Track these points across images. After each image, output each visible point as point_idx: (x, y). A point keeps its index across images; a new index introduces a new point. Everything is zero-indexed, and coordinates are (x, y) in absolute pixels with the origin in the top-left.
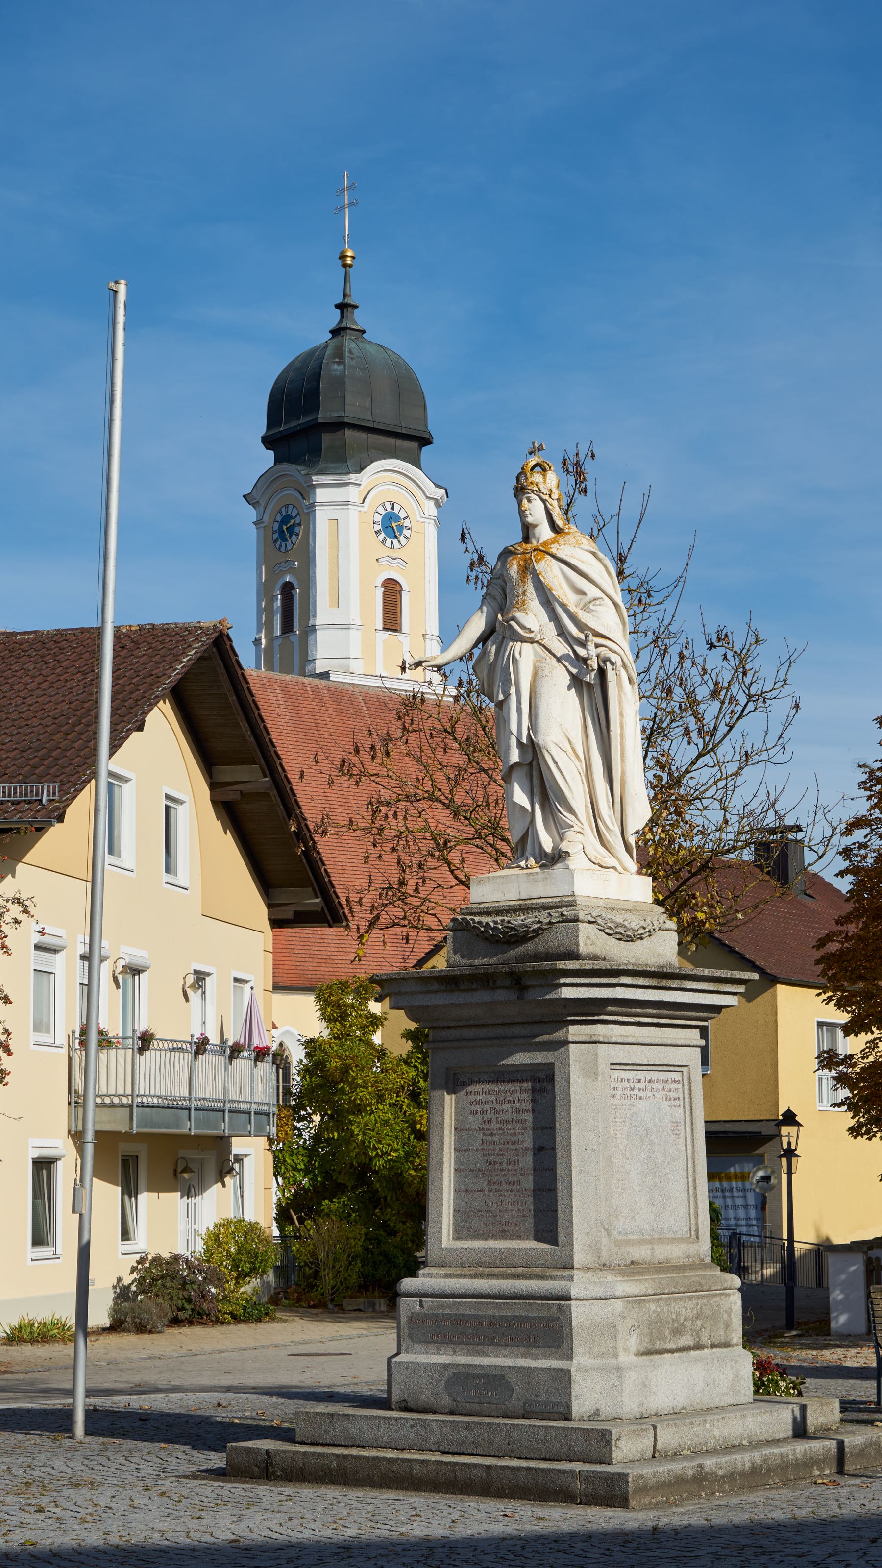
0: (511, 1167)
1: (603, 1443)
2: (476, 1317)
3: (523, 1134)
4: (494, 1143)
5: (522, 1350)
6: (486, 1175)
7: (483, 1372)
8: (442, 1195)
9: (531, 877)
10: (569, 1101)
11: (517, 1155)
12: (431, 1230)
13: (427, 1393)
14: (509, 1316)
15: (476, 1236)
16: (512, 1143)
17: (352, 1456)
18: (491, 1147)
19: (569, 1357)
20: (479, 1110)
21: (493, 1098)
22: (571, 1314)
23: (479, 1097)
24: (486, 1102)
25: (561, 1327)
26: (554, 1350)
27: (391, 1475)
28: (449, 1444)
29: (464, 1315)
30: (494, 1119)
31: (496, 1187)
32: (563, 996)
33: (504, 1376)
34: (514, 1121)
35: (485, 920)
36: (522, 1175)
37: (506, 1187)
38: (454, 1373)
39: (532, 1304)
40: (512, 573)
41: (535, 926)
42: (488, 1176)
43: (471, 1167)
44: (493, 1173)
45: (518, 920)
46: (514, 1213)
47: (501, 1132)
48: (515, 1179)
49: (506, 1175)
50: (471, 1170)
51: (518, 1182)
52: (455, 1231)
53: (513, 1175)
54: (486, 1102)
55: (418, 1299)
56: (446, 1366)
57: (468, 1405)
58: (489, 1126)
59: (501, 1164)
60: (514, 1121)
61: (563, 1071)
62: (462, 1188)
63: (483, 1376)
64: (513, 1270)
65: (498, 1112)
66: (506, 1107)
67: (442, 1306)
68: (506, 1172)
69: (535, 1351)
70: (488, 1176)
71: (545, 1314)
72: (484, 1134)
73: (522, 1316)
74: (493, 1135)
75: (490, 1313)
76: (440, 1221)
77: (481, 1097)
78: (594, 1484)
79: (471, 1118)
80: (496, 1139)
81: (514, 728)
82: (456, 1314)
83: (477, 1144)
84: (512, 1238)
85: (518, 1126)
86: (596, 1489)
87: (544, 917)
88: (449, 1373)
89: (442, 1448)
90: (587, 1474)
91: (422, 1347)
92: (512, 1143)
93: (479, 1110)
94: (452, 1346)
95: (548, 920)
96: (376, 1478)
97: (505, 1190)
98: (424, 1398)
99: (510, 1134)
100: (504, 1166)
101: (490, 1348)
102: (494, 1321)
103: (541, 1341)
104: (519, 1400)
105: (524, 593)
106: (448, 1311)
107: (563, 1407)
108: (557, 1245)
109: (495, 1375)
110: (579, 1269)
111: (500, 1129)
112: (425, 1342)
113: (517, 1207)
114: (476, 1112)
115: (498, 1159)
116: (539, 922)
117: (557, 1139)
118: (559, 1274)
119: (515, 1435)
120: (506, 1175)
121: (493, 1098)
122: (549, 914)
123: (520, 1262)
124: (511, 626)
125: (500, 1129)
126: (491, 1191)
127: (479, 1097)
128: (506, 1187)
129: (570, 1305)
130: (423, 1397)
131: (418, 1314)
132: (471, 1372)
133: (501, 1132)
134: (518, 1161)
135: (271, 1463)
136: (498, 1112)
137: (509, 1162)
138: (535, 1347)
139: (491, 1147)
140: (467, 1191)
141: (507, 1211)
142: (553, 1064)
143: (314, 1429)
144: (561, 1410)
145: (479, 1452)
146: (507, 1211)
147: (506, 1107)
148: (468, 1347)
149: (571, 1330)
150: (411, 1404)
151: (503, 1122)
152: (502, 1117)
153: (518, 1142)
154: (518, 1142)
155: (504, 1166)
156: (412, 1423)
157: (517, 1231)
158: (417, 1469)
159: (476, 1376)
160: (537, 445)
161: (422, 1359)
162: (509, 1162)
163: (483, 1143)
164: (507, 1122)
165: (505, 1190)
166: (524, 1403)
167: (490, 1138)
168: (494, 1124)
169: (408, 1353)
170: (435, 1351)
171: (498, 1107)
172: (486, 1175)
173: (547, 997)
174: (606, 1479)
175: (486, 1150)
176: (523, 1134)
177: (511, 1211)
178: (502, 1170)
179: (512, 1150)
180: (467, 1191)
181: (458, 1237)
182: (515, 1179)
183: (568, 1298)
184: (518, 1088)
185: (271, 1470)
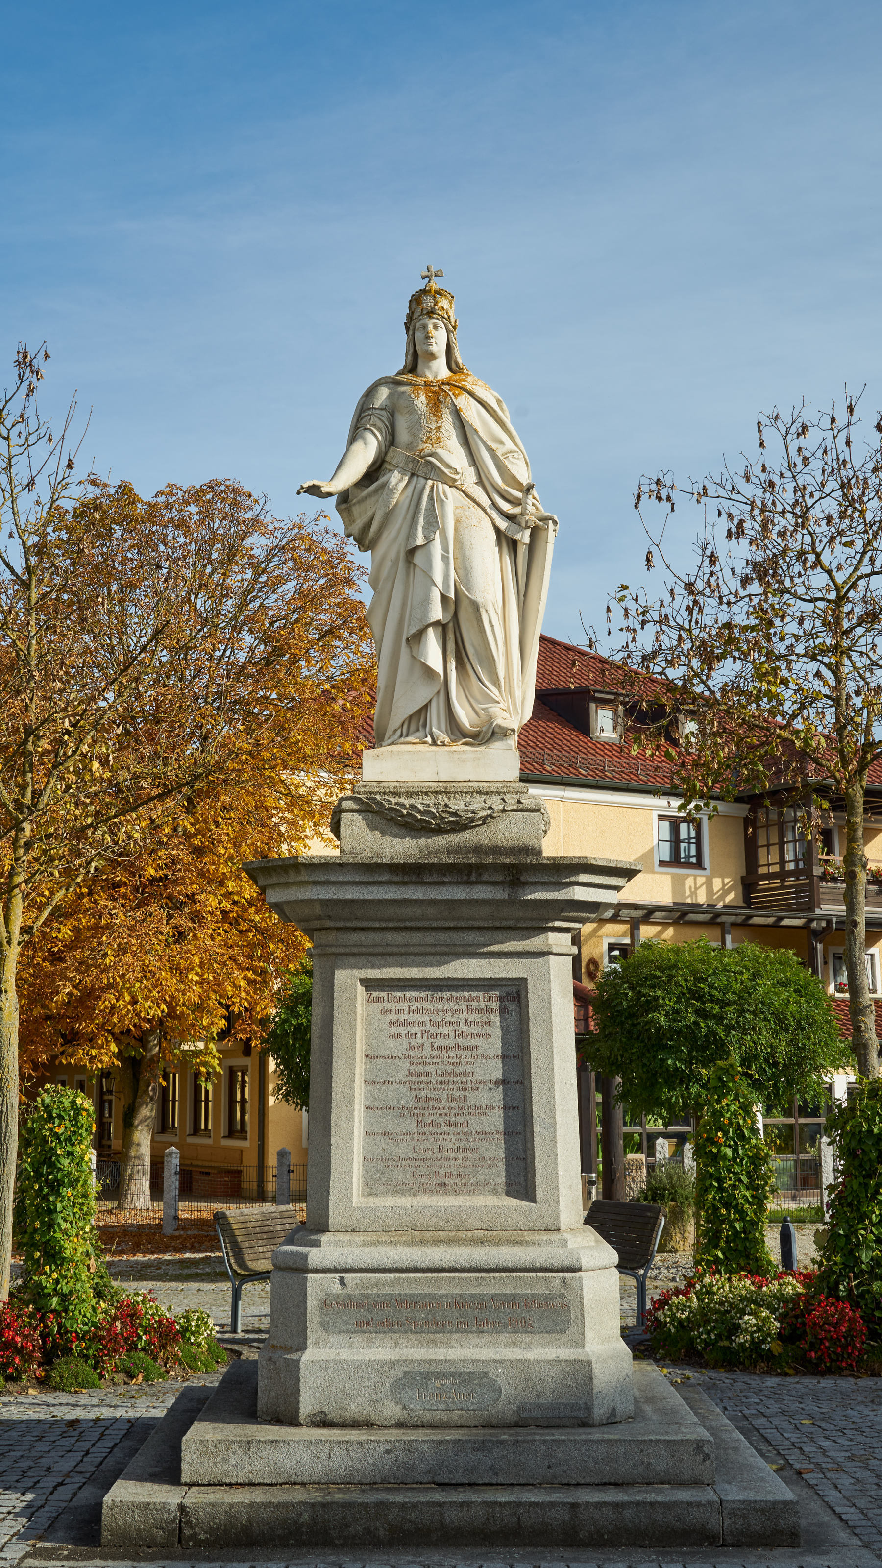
0: (453, 1104)
1: (700, 1458)
2: (433, 1297)
3: (473, 1063)
4: (427, 1074)
5: (505, 1337)
6: (414, 1115)
7: (453, 1369)
8: (352, 1139)
9: (456, 756)
10: (551, 1024)
11: (464, 1089)
12: (335, 1183)
13: (360, 1400)
14: (485, 1295)
15: (400, 1189)
16: (455, 1074)
17: (336, 1503)
18: (423, 1079)
19: (580, 1343)
20: (403, 1033)
21: (426, 1018)
22: (582, 1289)
23: (402, 1017)
24: (415, 1023)
25: (566, 1307)
26: (555, 1336)
27: (407, 1526)
28: (450, 1473)
29: (411, 1295)
30: (427, 1044)
31: (431, 1129)
32: (576, 898)
33: (486, 1373)
34: (457, 1047)
35: (417, 802)
36: (470, 1114)
37: (447, 1129)
38: (405, 1372)
39: (521, 1279)
40: (420, 405)
41: (484, 813)
42: (418, 1115)
43: (391, 1104)
44: (426, 1112)
45: (458, 805)
46: (458, 1162)
47: (438, 1060)
48: (461, 1119)
49: (445, 1114)
50: (390, 1108)
51: (466, 1124)
52: (366, 1185)
53: (456, 1115)
54: (415, 1023)
55: (337, 1275)
56: (392, 1364)
57: (427, 1413)
58: (418, 1053)
59: (439, 1100)
60: (457, 1047)
61: (540, 988)
62: (377, 1131)
63: (452, 1375)
64: (469, 1234)
65: (433, 1036)
66: (445, 1030)
67: (377, 1284)
68: (447, 1111)
69: (526, 1338)
70: (418, 1115)
71: (542, 1290)
72: (411, 1063)
73: (505, 1294)
74: (424, 1064)
75: (457, 1291)
76: (350, 1173)
77: (406, 1017)
78: (745, 1517)
79: (391, 1043)
80: (431, 1069)
81: (438, 577)
82: (400, 1295)
83: (402, 1075)
84: (456, 1192)
85: (464, 1053)
86: (749, 1525)
87: (477, 803)
88: (397, 1372)
89: (438, 1479)
90: (734, 1506)
91: (344, 1339)
92: (455, 1074)
93: (403, 1033)
94: (393, 1336)
95: (501, 807)
96: (382, 1532)
97: (444, 1134)
98: (354, 1409)
99: (453, 1064)
100: (444, 1103)
101: (456, 1336)
102: (459, 1303)
103: (535, 1325)
104: (510, 1403)
105: (438, 428)
106: (387, 1290)
107: (579, 1409)
108: (534, 1201)
109: (472, 1373)
110: (566, 1231)
111: (436, 1057)
112: (348, 1332)
113: (463, 1155)
114: (400, 1036)
115: (433, 1094)
116: (490, 808)
117: (533, 1071)
118: (545, 1238)
119: (560, 1455)
120: (445, 1114)
121: (426, 1018)
122: (503, 799)
123: (476, 1224)
124: (430, 463)
125: (436, 1057)
126: (424, 1133)
127: (402, 1017)
128: (447, 1129)
129: (581, 1278)
130: (353, 1406)
131: (338, 1296)
132: (432, 1369)
133: (438, 1060)
134: (465, 1097)
135: (189, 1523)
136: (433, 1036)
137: (451, 1099)
138: (526, 1332)
139: (423, 1079)
140: (384, 1134)
141: (447, 1159)
142: (524, 980)
143: (215, 1463)
144: (575, 1414)
145: (501, 1480)
146: (447, 1159)
147: (445, 1030)
148: (419, 1337)
149: (582, 1310)
150: (334, 1416)
151: (440, 1048)
152: (439, 1042)
153: (466, 1074)
154: (466, 1074)
155: (444, 1103)
156: (388, 1446)
157: (465, 1185)
158: (452, 1517)
159: (441, 1375)
160: (433, 270)
161: (346, 1354)
162: (451, 1099)
163: (410, 1074)
164: (448, 1048)
165: (444, 1134)
166: (519, 1407)
167: (420, 1068)
168: (427, 1051)
169: (318, 1347)
170: (364, 1344)
171: (433, 1030)
172: (414, 1115)
173: (529, 897)
174: (763, 1511)
175: (415, 1083)
176: (473, 1063)
177: (455, 1159)
178: (441, 1108)
179: (456, 1083)
180: (384, 1134)
181: (370, 1191)
182: (461, 1119)
183: (579, 1270)
184: (464, 1007)
185: (187, 1532)
